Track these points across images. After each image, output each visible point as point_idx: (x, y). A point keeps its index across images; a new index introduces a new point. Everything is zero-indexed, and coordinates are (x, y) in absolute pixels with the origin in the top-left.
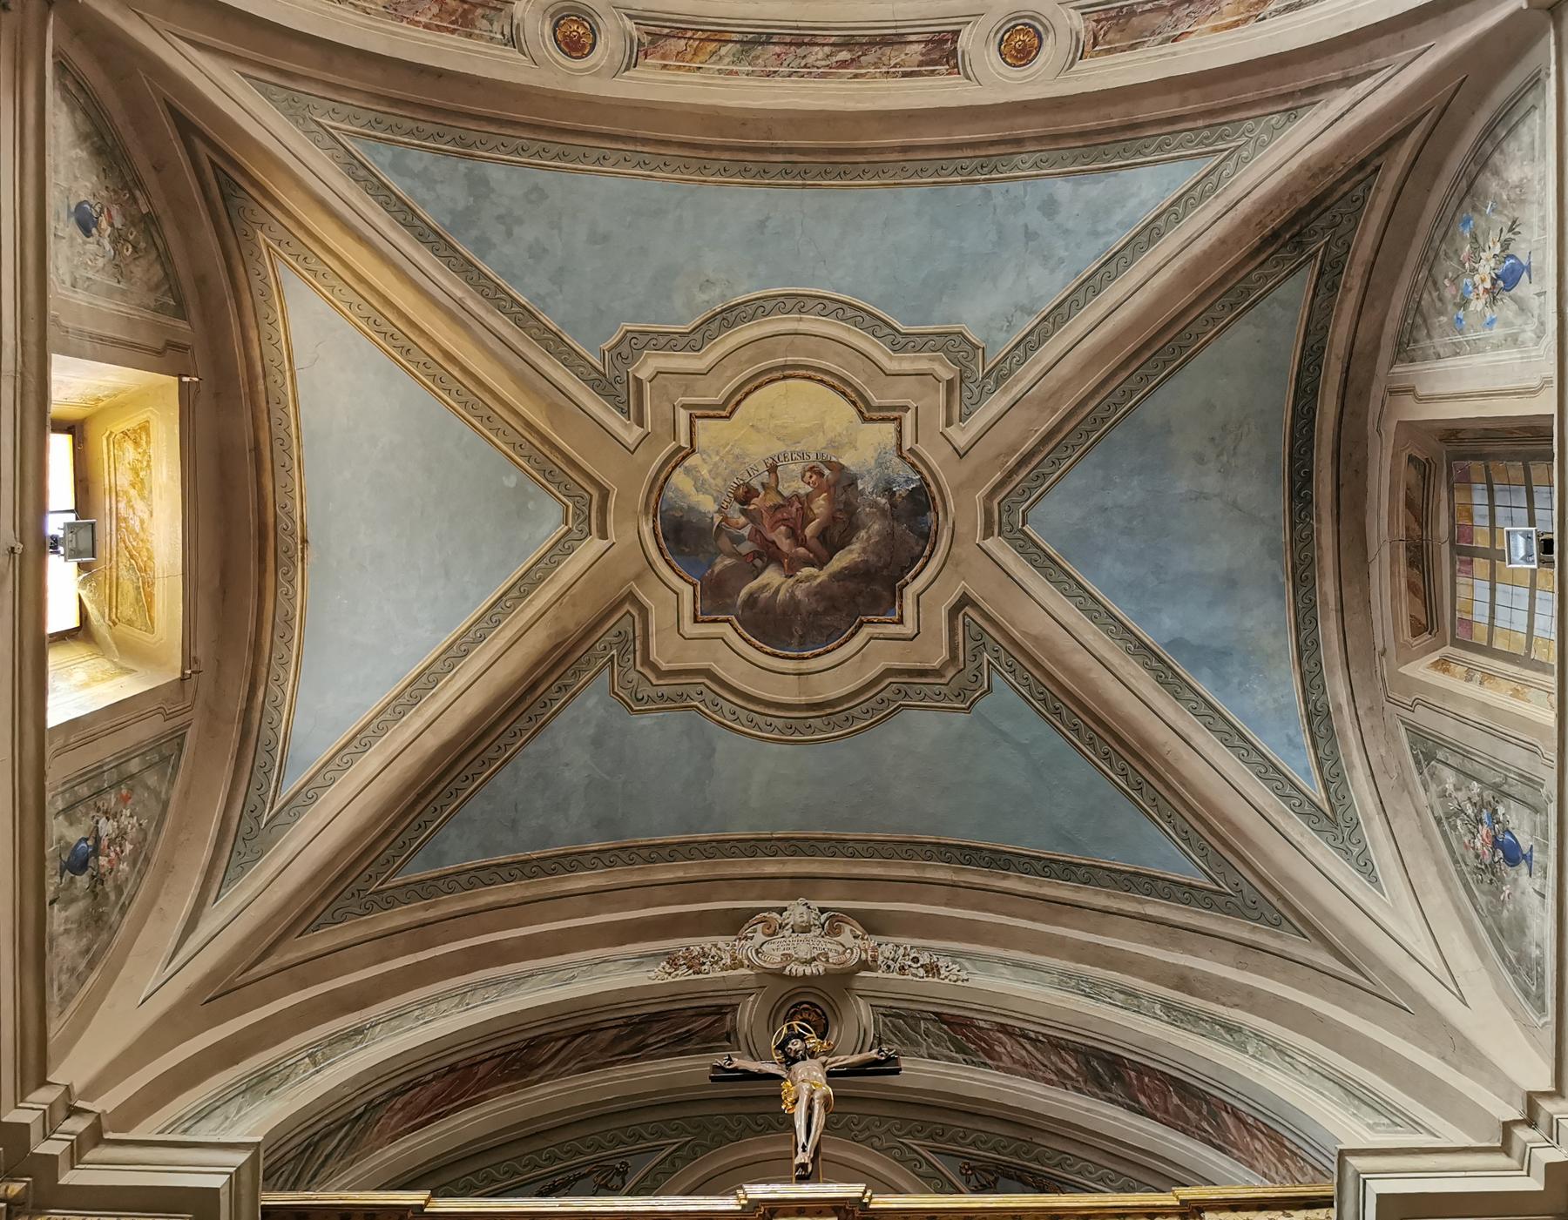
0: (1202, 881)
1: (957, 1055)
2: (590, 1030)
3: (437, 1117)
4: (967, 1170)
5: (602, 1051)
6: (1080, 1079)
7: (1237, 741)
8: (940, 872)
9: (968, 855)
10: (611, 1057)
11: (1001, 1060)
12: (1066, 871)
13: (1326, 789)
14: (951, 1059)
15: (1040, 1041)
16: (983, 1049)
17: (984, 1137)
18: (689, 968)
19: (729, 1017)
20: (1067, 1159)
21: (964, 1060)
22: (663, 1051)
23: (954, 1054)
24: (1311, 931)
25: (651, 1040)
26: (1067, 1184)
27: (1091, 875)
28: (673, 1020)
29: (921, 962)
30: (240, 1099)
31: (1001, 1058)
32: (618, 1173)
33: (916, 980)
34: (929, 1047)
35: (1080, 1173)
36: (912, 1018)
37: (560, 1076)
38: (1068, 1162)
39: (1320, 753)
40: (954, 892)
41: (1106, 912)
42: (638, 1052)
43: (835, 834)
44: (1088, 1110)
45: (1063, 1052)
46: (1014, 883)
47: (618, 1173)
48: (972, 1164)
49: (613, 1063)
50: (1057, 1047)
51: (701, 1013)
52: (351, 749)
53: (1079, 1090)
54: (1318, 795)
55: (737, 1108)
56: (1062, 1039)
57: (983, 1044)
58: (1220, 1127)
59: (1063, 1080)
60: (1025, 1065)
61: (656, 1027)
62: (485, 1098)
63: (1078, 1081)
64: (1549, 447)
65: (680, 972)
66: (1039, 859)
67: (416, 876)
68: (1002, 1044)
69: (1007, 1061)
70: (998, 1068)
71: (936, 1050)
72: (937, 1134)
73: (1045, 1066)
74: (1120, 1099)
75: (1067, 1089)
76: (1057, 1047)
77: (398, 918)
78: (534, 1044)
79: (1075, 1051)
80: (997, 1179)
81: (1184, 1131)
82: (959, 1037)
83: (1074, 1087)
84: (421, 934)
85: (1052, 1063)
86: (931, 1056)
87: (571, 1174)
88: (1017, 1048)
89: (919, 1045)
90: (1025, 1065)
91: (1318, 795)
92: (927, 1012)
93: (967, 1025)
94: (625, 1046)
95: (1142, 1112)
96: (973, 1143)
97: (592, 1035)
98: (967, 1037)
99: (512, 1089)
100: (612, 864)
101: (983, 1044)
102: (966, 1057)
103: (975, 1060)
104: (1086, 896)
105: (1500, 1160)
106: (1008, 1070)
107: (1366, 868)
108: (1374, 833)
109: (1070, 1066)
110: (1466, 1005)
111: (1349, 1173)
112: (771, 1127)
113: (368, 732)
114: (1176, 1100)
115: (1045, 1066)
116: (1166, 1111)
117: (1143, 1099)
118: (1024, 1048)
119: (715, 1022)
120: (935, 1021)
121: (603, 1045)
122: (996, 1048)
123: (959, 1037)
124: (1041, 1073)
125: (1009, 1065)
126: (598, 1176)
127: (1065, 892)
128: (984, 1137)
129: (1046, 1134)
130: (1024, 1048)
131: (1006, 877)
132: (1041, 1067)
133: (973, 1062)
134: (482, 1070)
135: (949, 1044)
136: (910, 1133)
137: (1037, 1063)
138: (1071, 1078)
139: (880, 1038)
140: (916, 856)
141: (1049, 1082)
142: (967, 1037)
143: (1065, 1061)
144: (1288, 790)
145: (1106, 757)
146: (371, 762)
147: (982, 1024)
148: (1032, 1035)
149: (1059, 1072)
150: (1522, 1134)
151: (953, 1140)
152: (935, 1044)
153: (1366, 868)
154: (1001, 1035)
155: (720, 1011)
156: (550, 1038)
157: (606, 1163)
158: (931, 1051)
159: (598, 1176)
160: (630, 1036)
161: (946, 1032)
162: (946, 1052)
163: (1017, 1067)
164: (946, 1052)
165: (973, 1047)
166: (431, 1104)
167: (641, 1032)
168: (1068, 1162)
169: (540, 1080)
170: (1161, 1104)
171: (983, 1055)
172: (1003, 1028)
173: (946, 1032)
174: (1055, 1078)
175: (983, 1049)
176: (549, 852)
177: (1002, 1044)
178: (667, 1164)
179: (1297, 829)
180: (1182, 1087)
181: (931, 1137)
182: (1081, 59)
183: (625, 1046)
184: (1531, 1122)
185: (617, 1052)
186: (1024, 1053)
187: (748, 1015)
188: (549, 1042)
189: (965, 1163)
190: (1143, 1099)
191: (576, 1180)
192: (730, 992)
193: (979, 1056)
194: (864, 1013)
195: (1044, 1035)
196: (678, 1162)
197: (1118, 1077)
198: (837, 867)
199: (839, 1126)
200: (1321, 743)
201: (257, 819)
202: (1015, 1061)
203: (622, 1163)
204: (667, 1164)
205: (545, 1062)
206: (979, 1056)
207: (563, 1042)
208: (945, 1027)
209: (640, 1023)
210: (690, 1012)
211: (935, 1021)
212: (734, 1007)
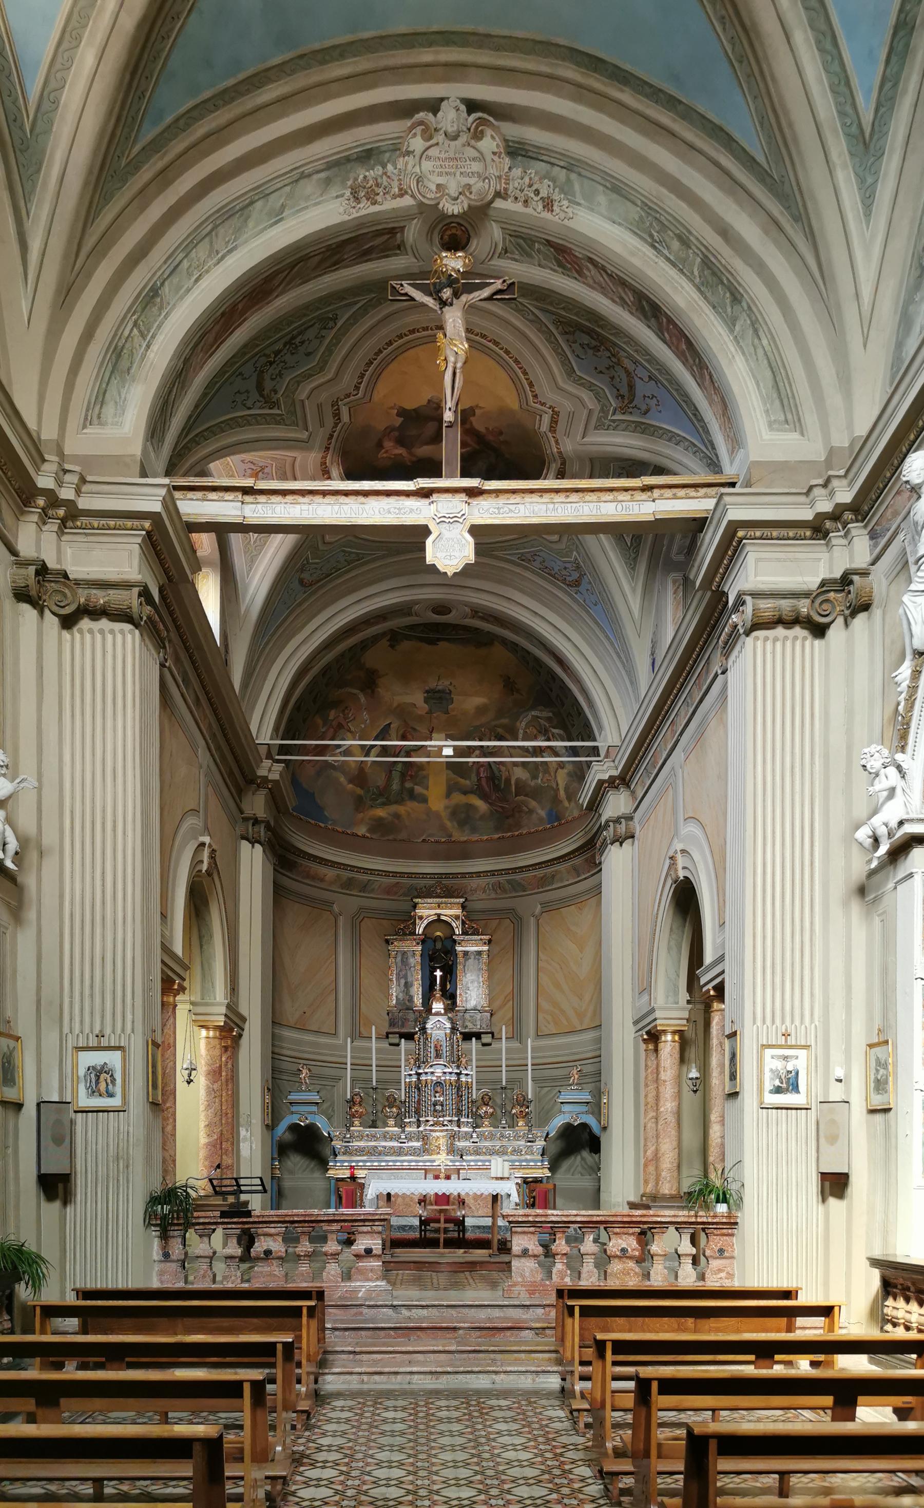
0: (761, 159)
2: (305, 259)
3: (221, 343)
7: (828, 46)
8: (569, 72)
9: (595, 64)
11: (586, 278)
12: (671, 103)
13: (877, 110)
14: (555, 271)
18: (368, 199)
19: (399, 235)
24: (811, 236)
27: (688, 114)
29: (541, 196)
30: (114, 382)
32: (331, 319)
33: (536, 210)
34: (539, 260)
36: (530, 240)
37: (289, 290)
39: (888, 70)
40: (580, 93)
41: (692, 147)
43: (481, 29)
46: (626, 97)
47: (331, 319)
49: (323, 274)
51: (379, 233)
52: (65, 45)
53: (632, 313)
54: (867, 117)
58: (702, 376)
59: (623, 303)
64: (279, 1347)
65: (361, 205)
66: (651, 86)
67: (150, 137)
69: (591, 282)
70: (584, 283)
71: (544, 262)
77: (146, 174)
78: (268, 280)
84: (164, 178)
86: (539, 265)
91: (867, 117)
95: (665, 342)
96: (563, 308)
100: (293, 72)
104: (678, 126)
105: (803, 499)
107: (868, 228)
108: (891, 164)
109: (630, 297)
110: (865, 346)
111: (722, 502)
113: (73, 23)
114: (684, 347)
116: (677, 348)
117: (666, 335)
119: (389, 239)
127: (665, 118)
131: (622, 91)
134: (240, 306)
138: (629, 305)
141: (614, 301)
145: (722, 19)
146: (87, 57)
147: (577, 254)
149: (621, 298)
150: (817, 491)
151: (551, 304)
153: (868, 228)
155: (392, 232)
156: (277, 273)
163: (595, 285)
166: (216, 340)
169: (277, 296)
170: (675, 343)
172: (591, 260)
176: (241, 76)
179: (839, 147)
180: (689, 343)
181: (536, 300)
184: (825, 486)
187: (413, 233)
188: (278, 274)
190: (666, 335)
194: (496, 232)
195: (617, 275)
197: (656, 317)
198: (484, 57)
200: (894, 59)
201: (22, 128)
202: (595, 282)
205: (279, 285)
207: (286, 272)
209: (337, 247)
210: (370, 235)
212: (402, 228)
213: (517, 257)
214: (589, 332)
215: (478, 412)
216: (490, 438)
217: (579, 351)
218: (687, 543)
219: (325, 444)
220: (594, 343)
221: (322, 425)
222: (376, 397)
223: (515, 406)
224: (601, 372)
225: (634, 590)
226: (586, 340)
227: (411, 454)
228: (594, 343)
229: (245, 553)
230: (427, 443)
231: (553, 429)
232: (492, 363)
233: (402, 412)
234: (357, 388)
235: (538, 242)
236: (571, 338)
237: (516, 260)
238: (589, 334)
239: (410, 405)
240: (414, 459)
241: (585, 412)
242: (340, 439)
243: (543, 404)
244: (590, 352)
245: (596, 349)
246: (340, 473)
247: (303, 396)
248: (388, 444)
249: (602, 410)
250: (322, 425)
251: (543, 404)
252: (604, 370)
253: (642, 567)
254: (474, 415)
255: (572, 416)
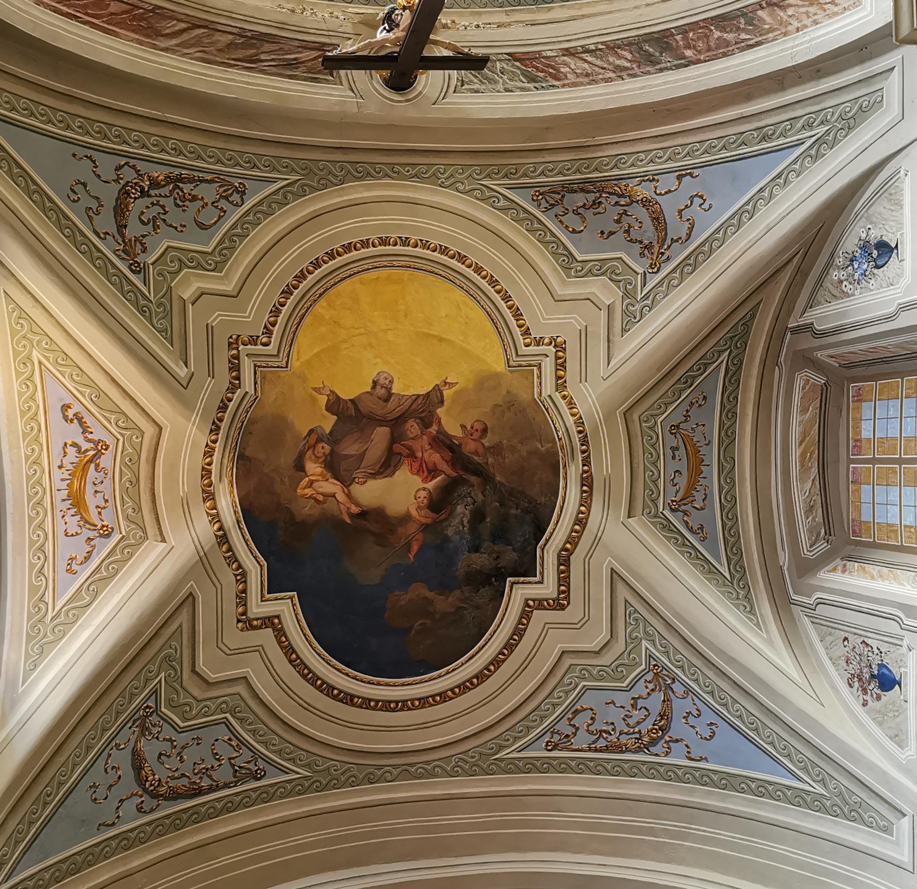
1: (529, 85)
4: (538, 196)
5: (219, 50)
6: (634, 66)
10: (228, 59)
14: (523, 89)
15: (600, 50)
16: (550, 74)
17: (551, 166)
20: (621, 159)
21: (535, 87)
22: (274, 70)
23: (526, 85)
25: (263, 57)
26: (622, 179)
28: (281, 46)
31: (566, 76)
34: (504, 83)
35: (633, 165)
38: (623, 161)
42: (251, 63)
44: (643, 88)
45: (619, 51)
48: (542, 190)
50: (613, 48)
53: (634, 76)
55: (338, 157)
56: (618, 40)
57: (551, 70)
60: (587, 75)
61: (267, 47)
62: (116, 34)
63: (632, 68)
68: (566, 64)
71: (510, 85)
72: (511, 173)
73: (604, 68)
74: (669, 64)
75: (623, 79)
76: (613, 48)
79: (630, 44)
80: (563, 196)
81: (725, 55)
82: (530, 70)
83: (629, 75)
85: (610, 64)
86: (507, 90)
87: (196, 174)
88: (580, 64)
89: (496, 82)
90: (587, 75)
92: (502, 54)
93: (537, 58)
94: (240, 54)
96: (542, 173)
97: (212, 32)
98: (537, 68)
99: (141, 43)
101: (551, 70)
102: (537, 85)
103: (544, 85)
106: (574, 85)
112: (369, 174)
114: (717, 34)
115: (604, 68)
118: (586, 61)
120: (509, 60)
121: (220, 46)
122: (562, 70)
123: (530, 70)
124: (601, 76)
125: (573, 80)
126: (220, 187)
128: (551, 166)
129: (604, 147)
130: (586, 61)
132: (602, 71)
133: (543, 87)
135: (521, 77)
136: (488, 176)
137: (597, 69)
138: (626, 69)
139: (462, 80)
140: (473, 5)
142: (537, 68)
143: (620, 57)
144: (706, 248)
147: (549, 54)
148: (592, 47)
151: (525, 175)
152: (510, 80)
154: (565, 58)
157: (227, 178)
158: (507, 86)
159: (220, 187)
160: (244, 46)
161: (518, 68)
162: (519, 84)
163: (580, 80)
164: (519, 84)
165: (542, 75)
167: (252, 46)
168: (623, 161)
171: (550, 79)
172: (568, 52)
173: (518, 68)
174: (612, 75)
175: (550, 74)
177: (566, 64)
178: (279, 197)
182: (454, 92)
183: (240, 54)
185: (233, 57)
186: (586, 65)
189: (536, 191)
191: (201, 181)
192: (331, 33)
193: (547, 81)
196: (289, 196)
199: (425, 176)
203: (240, 183)
204: (279, 197)
206: (547, 81)
208: (518, 64)
209: (252, 38)
210: (296, 43)
211: (509, 60)
213: (476, 87)
214: (583, 187)
215: (447, 393)
216: (470, 447)
217: (571, 220)
218: (819, 519)
219: (213, 415)
220: (591, 197)
221: (211, 374)
222: (295, 363)
223: (500, 367)
224: (611, 233)
225: (770, 642)
226: (580, 199)
227: (349, 496)
228: (591, 197)
229: (29, 638)
230: (374, 475)
231: (561, 383)
232: (459, 295)
233: (335, 405)
234: (268, 332)
235: (500, 60)
236: (558, 210)
237: (477, 91)
238: (582, 190)
239: (347, 394)
240: (355, 509)
241: (603, 314)
242: (237, 424)
243: (539, 342)
244: (589, 214)
245: (596, 204)
246: (233, 501)
247: (187, 294)
248: (313, 468)
249: (627, 294)
250: (211, 374)
251: (539, 342)
252: (614, 227)
253: (765, 608)
254: (442, 402)
255: (583, 335)
